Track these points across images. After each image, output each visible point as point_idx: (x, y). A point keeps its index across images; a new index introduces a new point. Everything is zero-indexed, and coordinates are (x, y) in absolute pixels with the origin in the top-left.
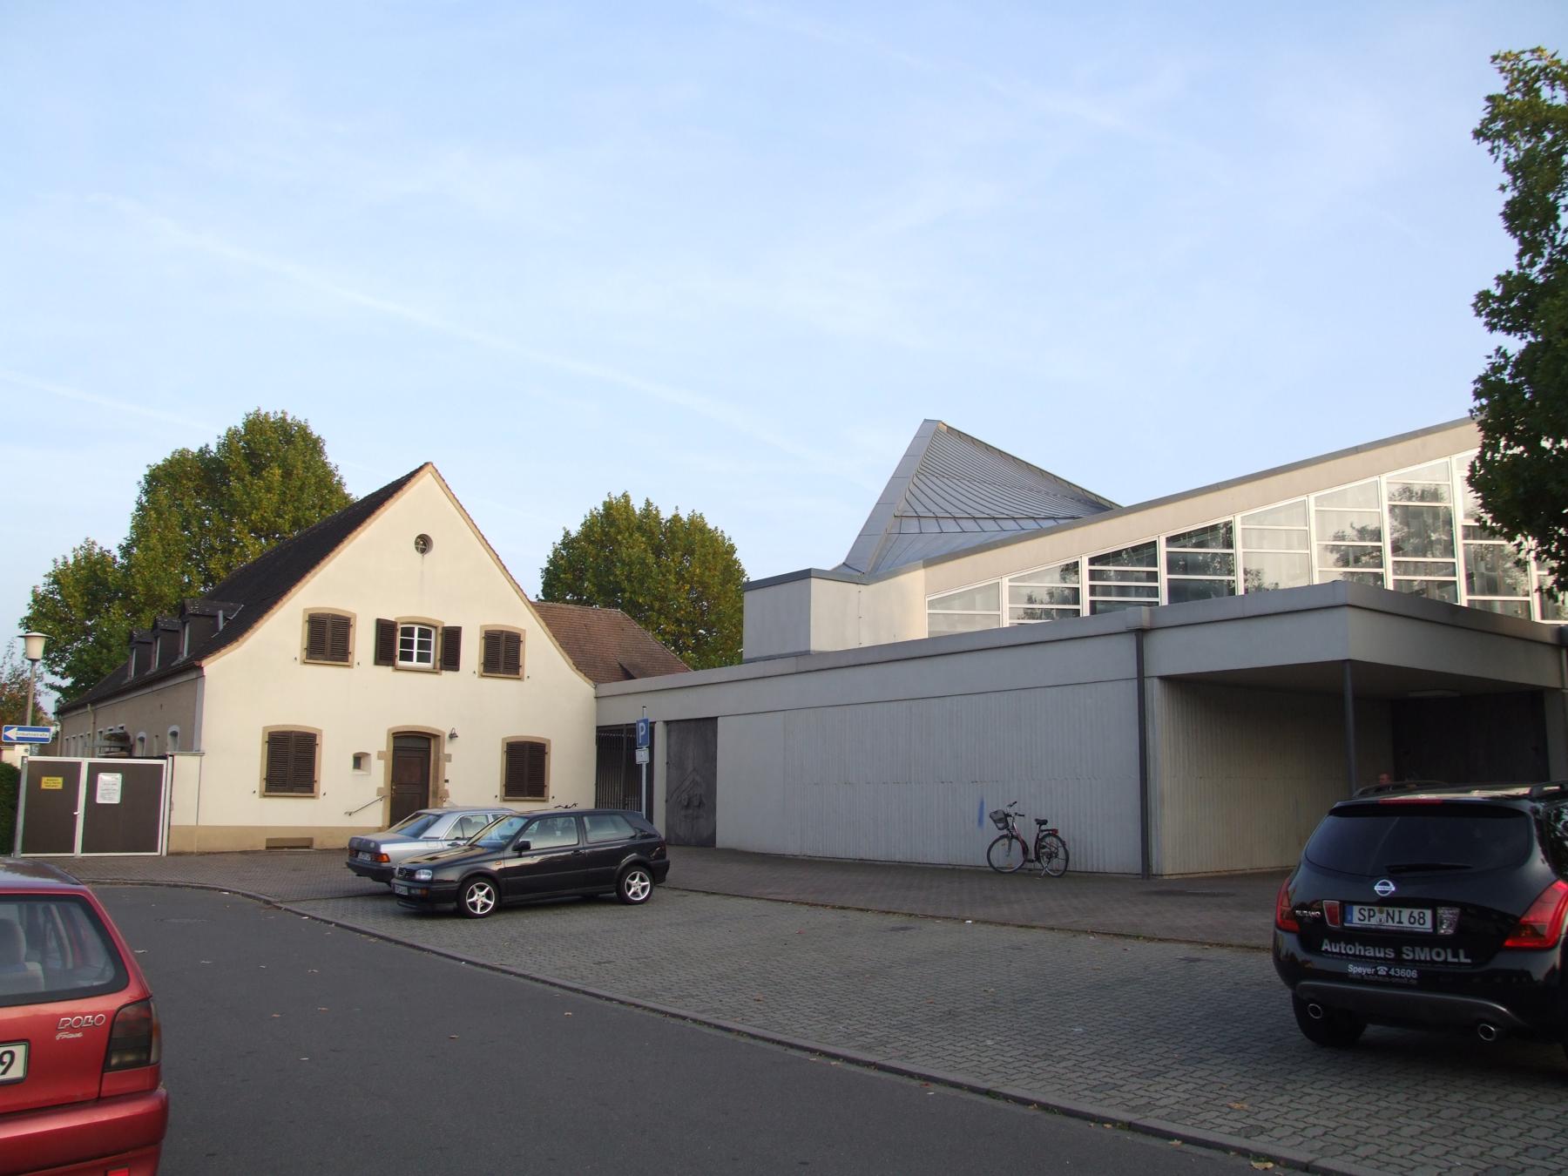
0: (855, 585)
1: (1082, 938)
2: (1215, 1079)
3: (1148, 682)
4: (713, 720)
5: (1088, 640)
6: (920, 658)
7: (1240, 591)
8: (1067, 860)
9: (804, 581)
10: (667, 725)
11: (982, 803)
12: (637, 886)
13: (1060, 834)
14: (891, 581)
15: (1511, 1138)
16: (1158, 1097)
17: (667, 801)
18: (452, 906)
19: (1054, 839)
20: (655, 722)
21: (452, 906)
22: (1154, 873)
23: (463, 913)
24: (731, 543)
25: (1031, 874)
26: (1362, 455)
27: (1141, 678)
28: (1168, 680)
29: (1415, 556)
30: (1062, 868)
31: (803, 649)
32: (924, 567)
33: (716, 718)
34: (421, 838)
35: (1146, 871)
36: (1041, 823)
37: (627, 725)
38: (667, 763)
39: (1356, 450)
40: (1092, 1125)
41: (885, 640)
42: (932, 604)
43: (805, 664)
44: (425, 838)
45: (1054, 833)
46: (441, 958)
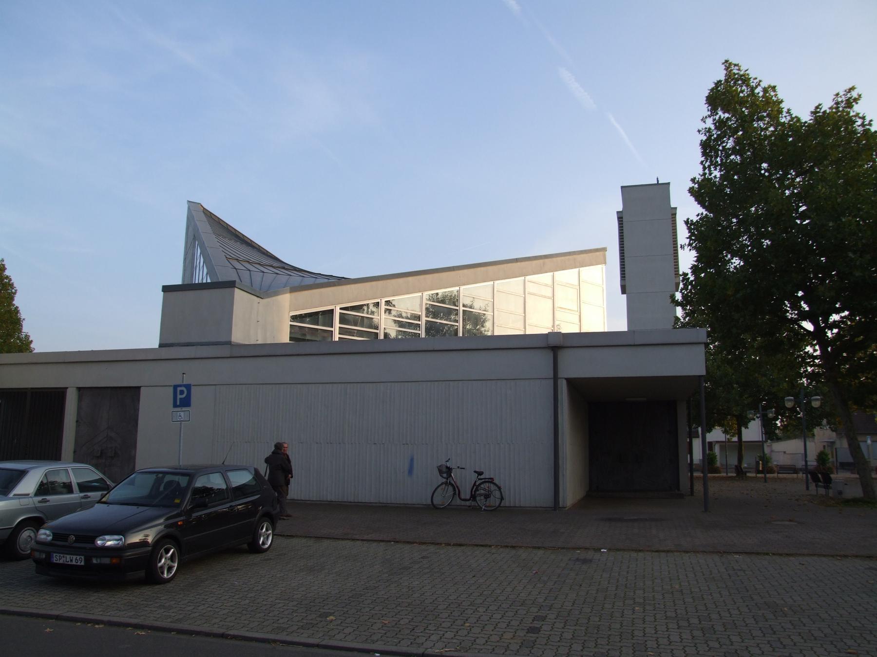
0: (255, 297)
1: (358, 542)
2: (238, 600)
3: (559, 381)
4: (138, 389)
5: (398, 355)
6: (323, 354)
7: (461, 334)
8: (502, 499)
9: (228, 290)
10: (79, 391)
11: (412, 460)
12: (266, 538)
13: (496, 481)
14: (274, 298)
15: (403, 619)
16: (165, 613)
17: (75, 452)
18: (142, 574)
19: (492, 485)
20: (67, 388)
21: (142, 574)
22: (561, 506)
23: (153, 578)
24: (3, 263)
25: (476, 509)
26: (519, 263)
27: (556, 378)
28: (570, 381)
29: (409, 329)
30: (497, 504)
31: (223, 339)
32: (290, 292)
33: (138, 388)
34: (11, 495)
35: (556, 505)
36: (480, 473)
37: (32, 388)
38: (77, 421)
39: (516, 260)
40: (149, 631)
41: (269, 341)
42: (294, 318)
43: (225, 351)
44: (15, 495)
45: (491, 481)
46: (254, 644)
